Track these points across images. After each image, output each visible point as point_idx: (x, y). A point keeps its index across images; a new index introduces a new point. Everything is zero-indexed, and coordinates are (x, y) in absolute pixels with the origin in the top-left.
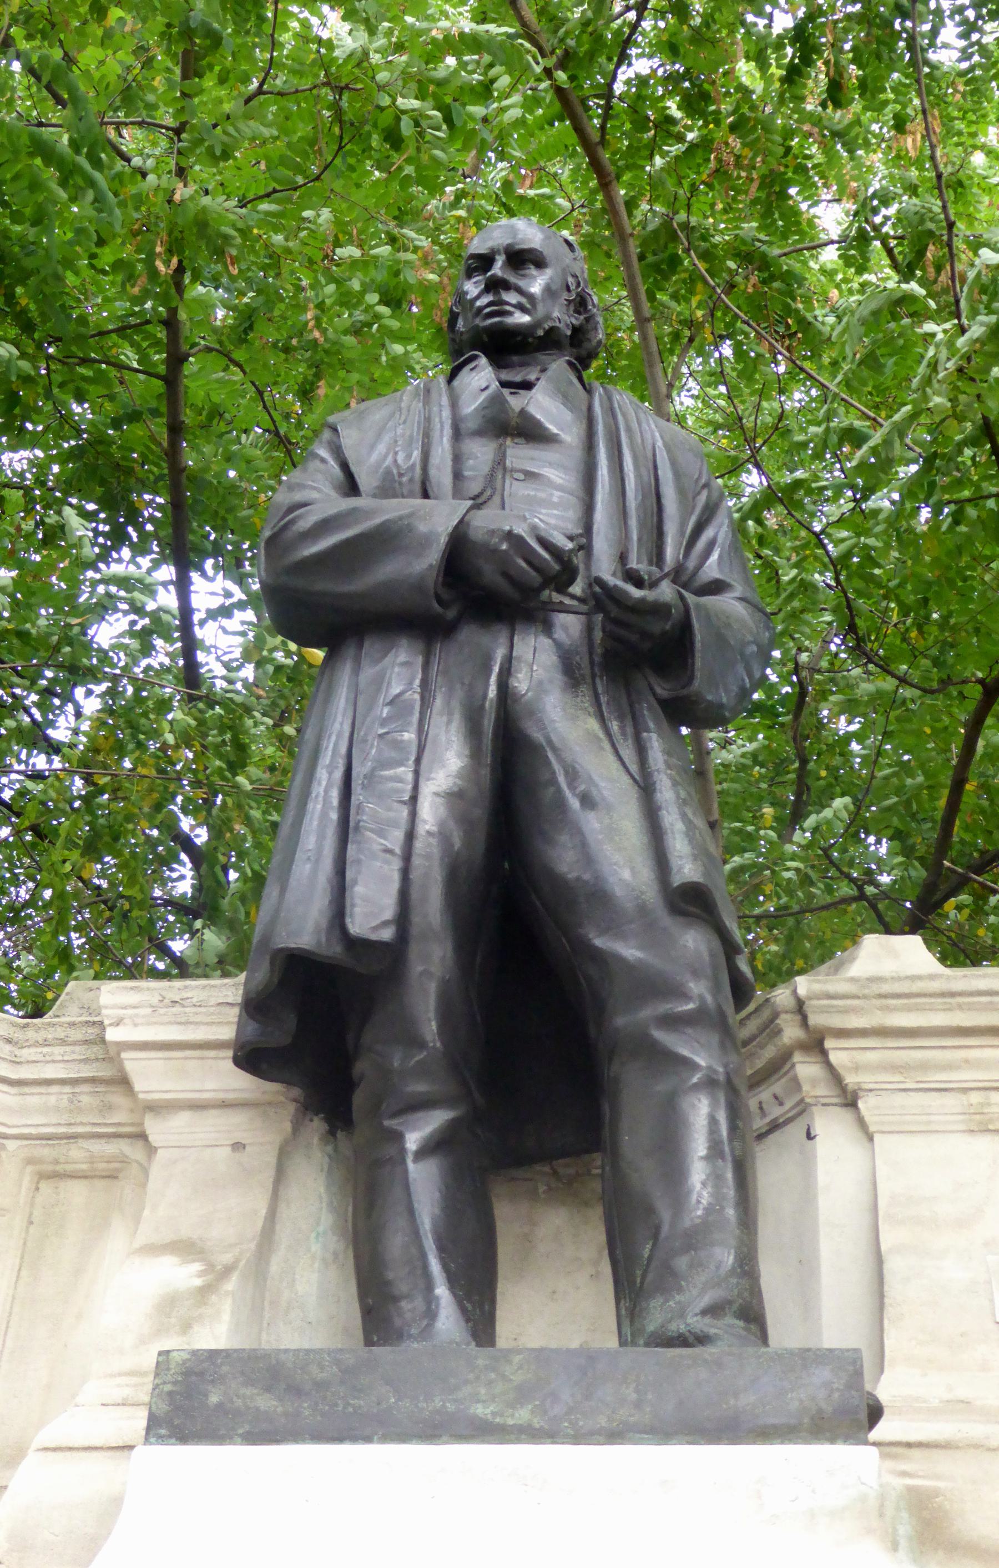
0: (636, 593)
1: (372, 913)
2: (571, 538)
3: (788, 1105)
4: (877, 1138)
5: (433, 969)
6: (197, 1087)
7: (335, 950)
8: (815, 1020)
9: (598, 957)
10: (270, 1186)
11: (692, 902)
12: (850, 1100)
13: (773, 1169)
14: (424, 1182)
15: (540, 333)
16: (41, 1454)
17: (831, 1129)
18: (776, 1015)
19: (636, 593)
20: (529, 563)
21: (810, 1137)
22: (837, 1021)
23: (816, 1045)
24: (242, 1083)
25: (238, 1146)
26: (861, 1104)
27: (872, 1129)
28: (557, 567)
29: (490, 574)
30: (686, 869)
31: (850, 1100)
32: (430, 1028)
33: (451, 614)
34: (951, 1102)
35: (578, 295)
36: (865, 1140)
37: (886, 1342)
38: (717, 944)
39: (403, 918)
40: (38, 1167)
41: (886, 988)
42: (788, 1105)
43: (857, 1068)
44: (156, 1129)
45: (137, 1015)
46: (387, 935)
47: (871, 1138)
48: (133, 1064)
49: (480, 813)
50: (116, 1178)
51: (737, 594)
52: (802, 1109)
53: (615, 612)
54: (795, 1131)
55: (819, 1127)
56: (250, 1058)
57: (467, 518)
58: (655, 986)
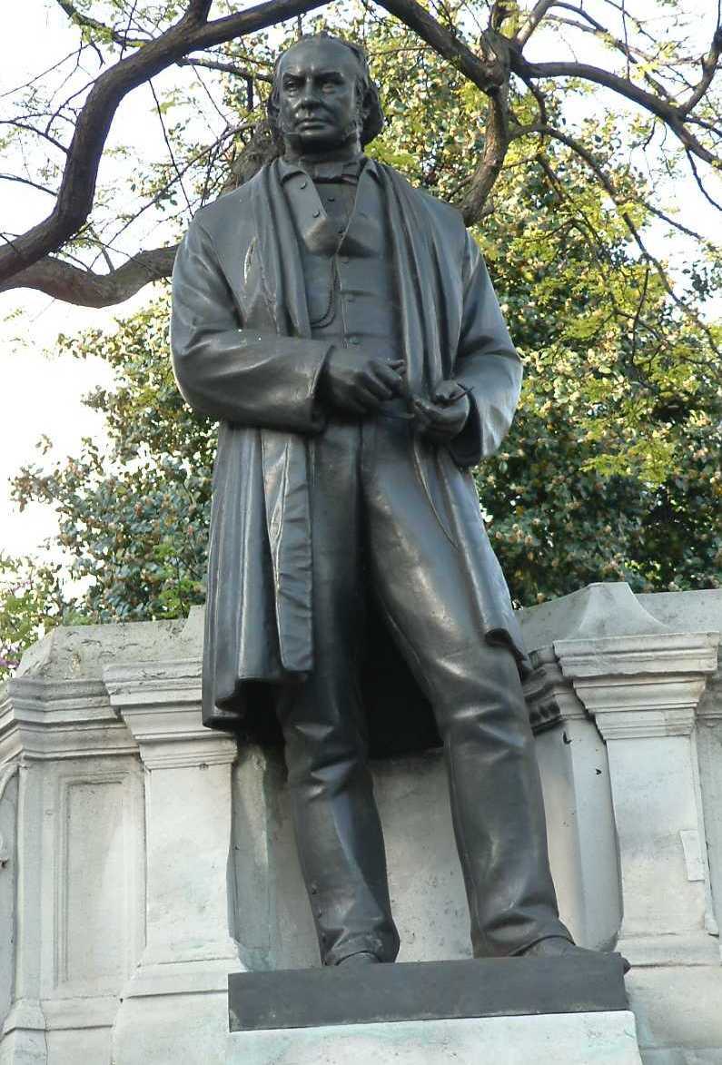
6: (175, 730)
7: (276, 674)
17: (576, 731)
24: (209, 732)
27: (605, 738)
39: (316, 654)
40: (67, 780)
43: (593, 700)
46: (308, 665)
47: (605, 743)
50: (120, 783)
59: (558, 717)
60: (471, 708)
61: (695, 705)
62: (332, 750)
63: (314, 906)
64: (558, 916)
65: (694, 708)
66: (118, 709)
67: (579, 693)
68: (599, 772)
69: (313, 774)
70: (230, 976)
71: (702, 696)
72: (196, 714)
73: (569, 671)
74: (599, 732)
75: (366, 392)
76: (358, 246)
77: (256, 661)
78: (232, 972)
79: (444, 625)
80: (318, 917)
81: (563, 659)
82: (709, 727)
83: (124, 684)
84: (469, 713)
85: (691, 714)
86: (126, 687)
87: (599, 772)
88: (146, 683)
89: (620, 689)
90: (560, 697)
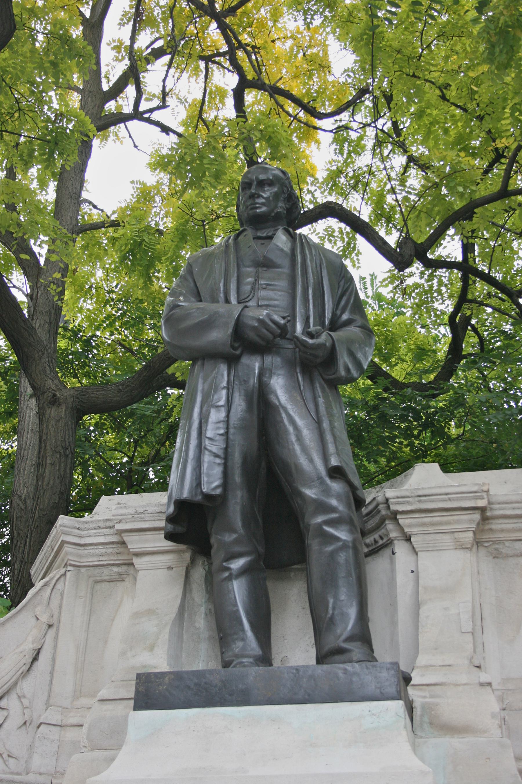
0: (310, 341)
1: (212, 483)
2: (284, 318)
3: (385, 540)
4: (419, 553)
5: (238, 501)
6: (152, 546)
7: (199, 498)
8: (393, 507)
9: (301, 495)
10: (183, 585)
11: (336, 473)
12: (408, 539)
13: (376, 568)
14: (238, 590)
15: (273, 214)
16: (100, 702)
17: (401, 549)
18: (378, 505)
19: (310, 341)
20: (267, 330)
21: (393, 553)
22: (400, 508)
23: (394, 516)
24: (169, 545)
25: (170, 568)
26: (412, 539)
27: (417, 550)
28: (279, 331)
29: (252, 335)
30: (334, 462)
31: (408, 539)
32: (238, 523)
33: (238, 352)
34: (447, 537)
35: (288, 194)
36: (415, 555)
37: (420, 641)
38: (347, 489)
39: (225, 484)
40: (94, 579)
41: (420, 493)
42: (385, 540)
43: (410, 526)
44: (136, 561)
45: (127, 519)
46: (218, 491)
47: (417, 554)
48: (127, 538)
49: (254, 433)
50: (124, 581)
51: (359, 324)
52: (389, 543)
53: (302, 348)
54: (387, 552)
55: (396, 550)
56: (170, 537)
57: (242, 313)
58: (323, 507)
59: (390, 539)
60: (319, 517)
61: (474, 529)
62: (237, 549)
63: (221, 647)
64: (373, 652)
65: (473, 531)
66: (121, 532)
67: (400, 521)
68: (413, 572)
69: (224, 564)
70: (138, 675)
71: (478, 524)
72: (161, 535)
73: (393, 507)
74: (413, 548)
75: (264, 331)
76: (271, 261)
77: (190, 491)
78: (138, 672)
79: (305, 467)
80: (222, 653)
81: (390, 500)
82: (486, 547)
83: (124, 517)
84: (319, 519)
85: (471, 535)
86: (124, 519)
87: (413, 572)
88: (136, 516)
89: (427, 519)
90: (390, 525)
